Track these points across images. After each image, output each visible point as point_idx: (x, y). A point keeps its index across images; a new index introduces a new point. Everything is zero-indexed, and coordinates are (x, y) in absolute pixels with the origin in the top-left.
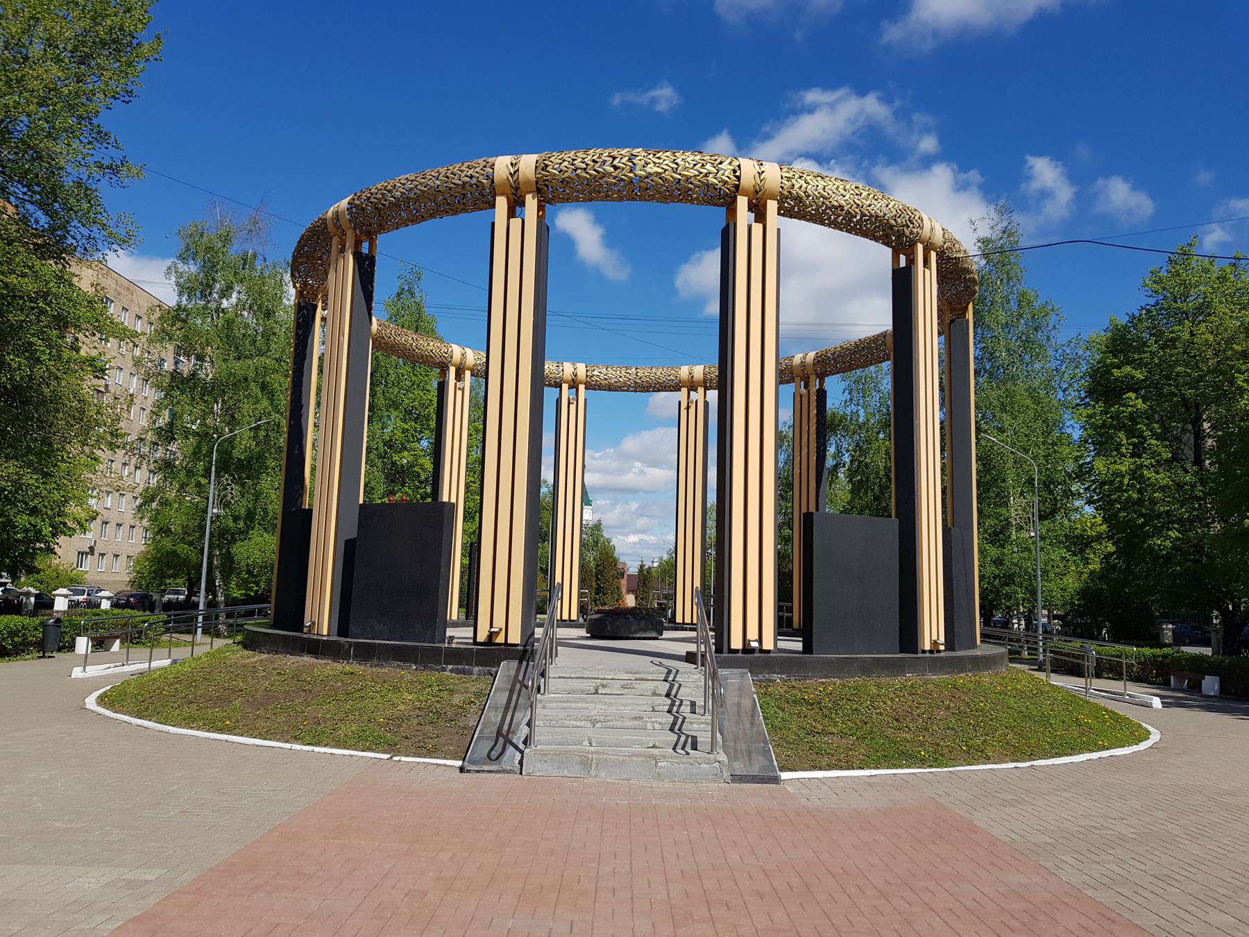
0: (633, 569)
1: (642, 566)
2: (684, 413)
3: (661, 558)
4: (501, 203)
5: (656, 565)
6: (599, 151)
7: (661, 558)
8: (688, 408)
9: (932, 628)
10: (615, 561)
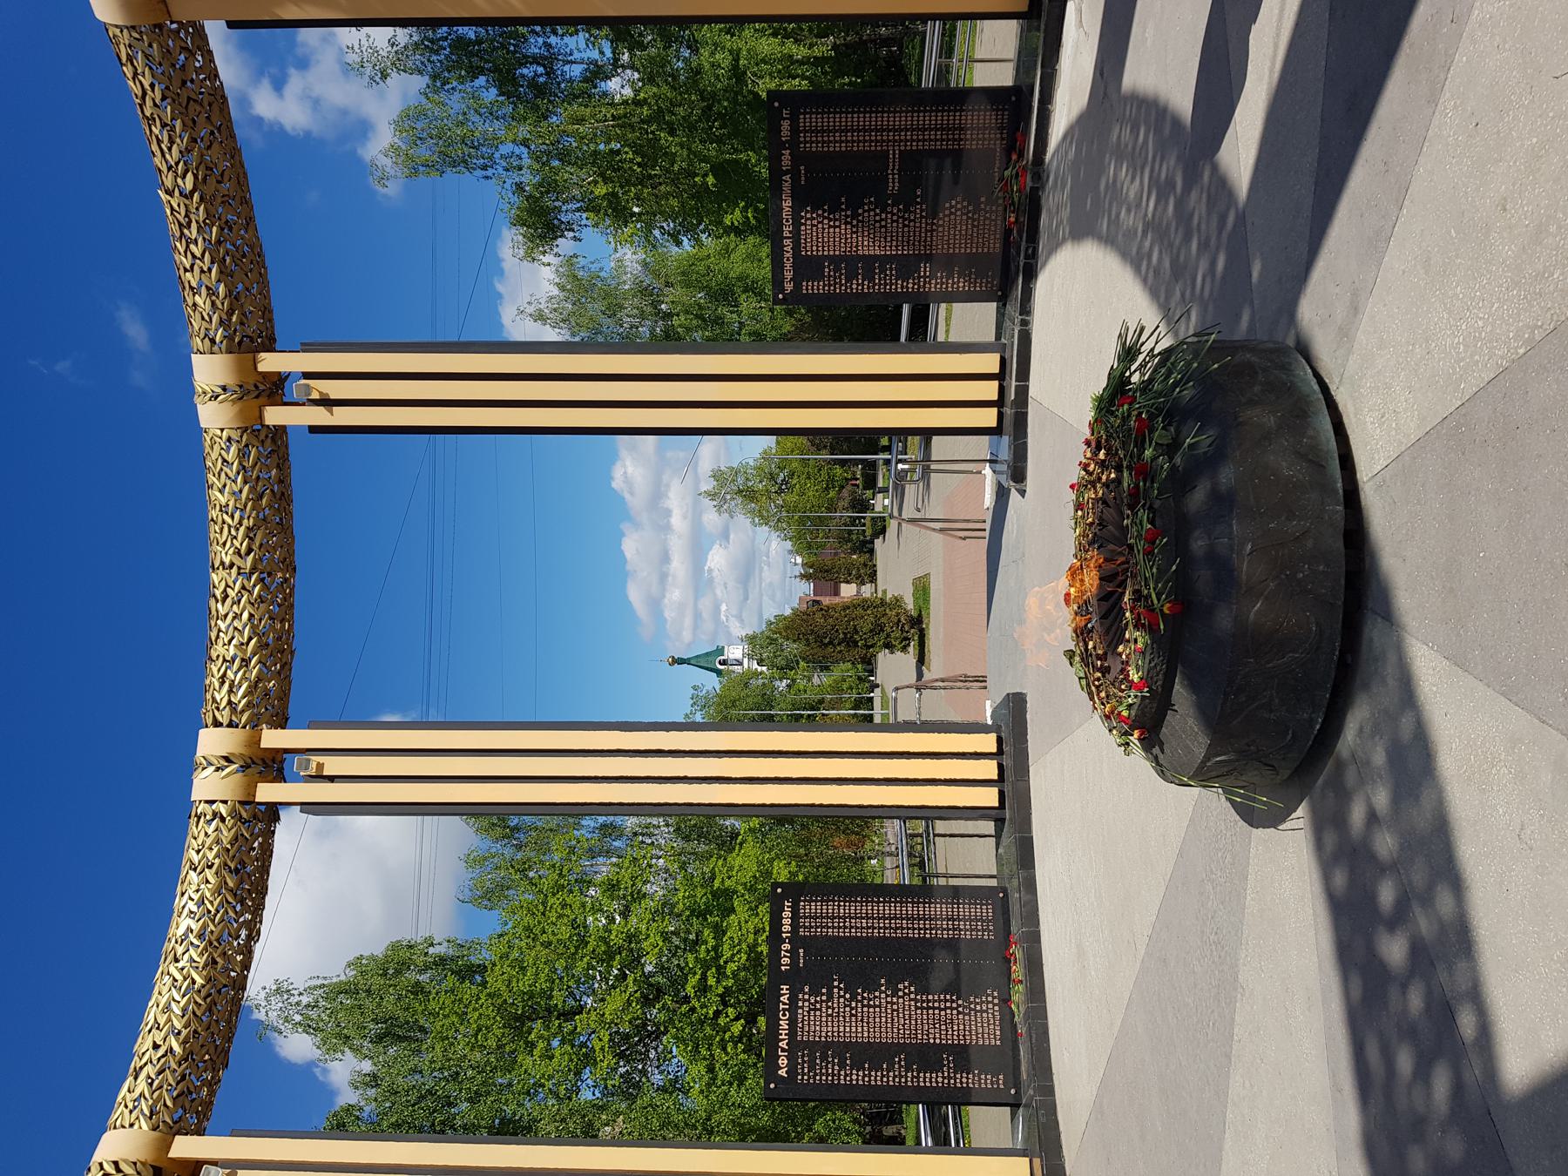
0: (807, 588)
1: (802, 576)
2: (343, 416)
3: (790, 552)
4: (275, 416)
5: (799, 560)
6: (214, 513)
7: (790, 552)
8: (327, 403)
9: (906, 309)
10: (796, 612)
